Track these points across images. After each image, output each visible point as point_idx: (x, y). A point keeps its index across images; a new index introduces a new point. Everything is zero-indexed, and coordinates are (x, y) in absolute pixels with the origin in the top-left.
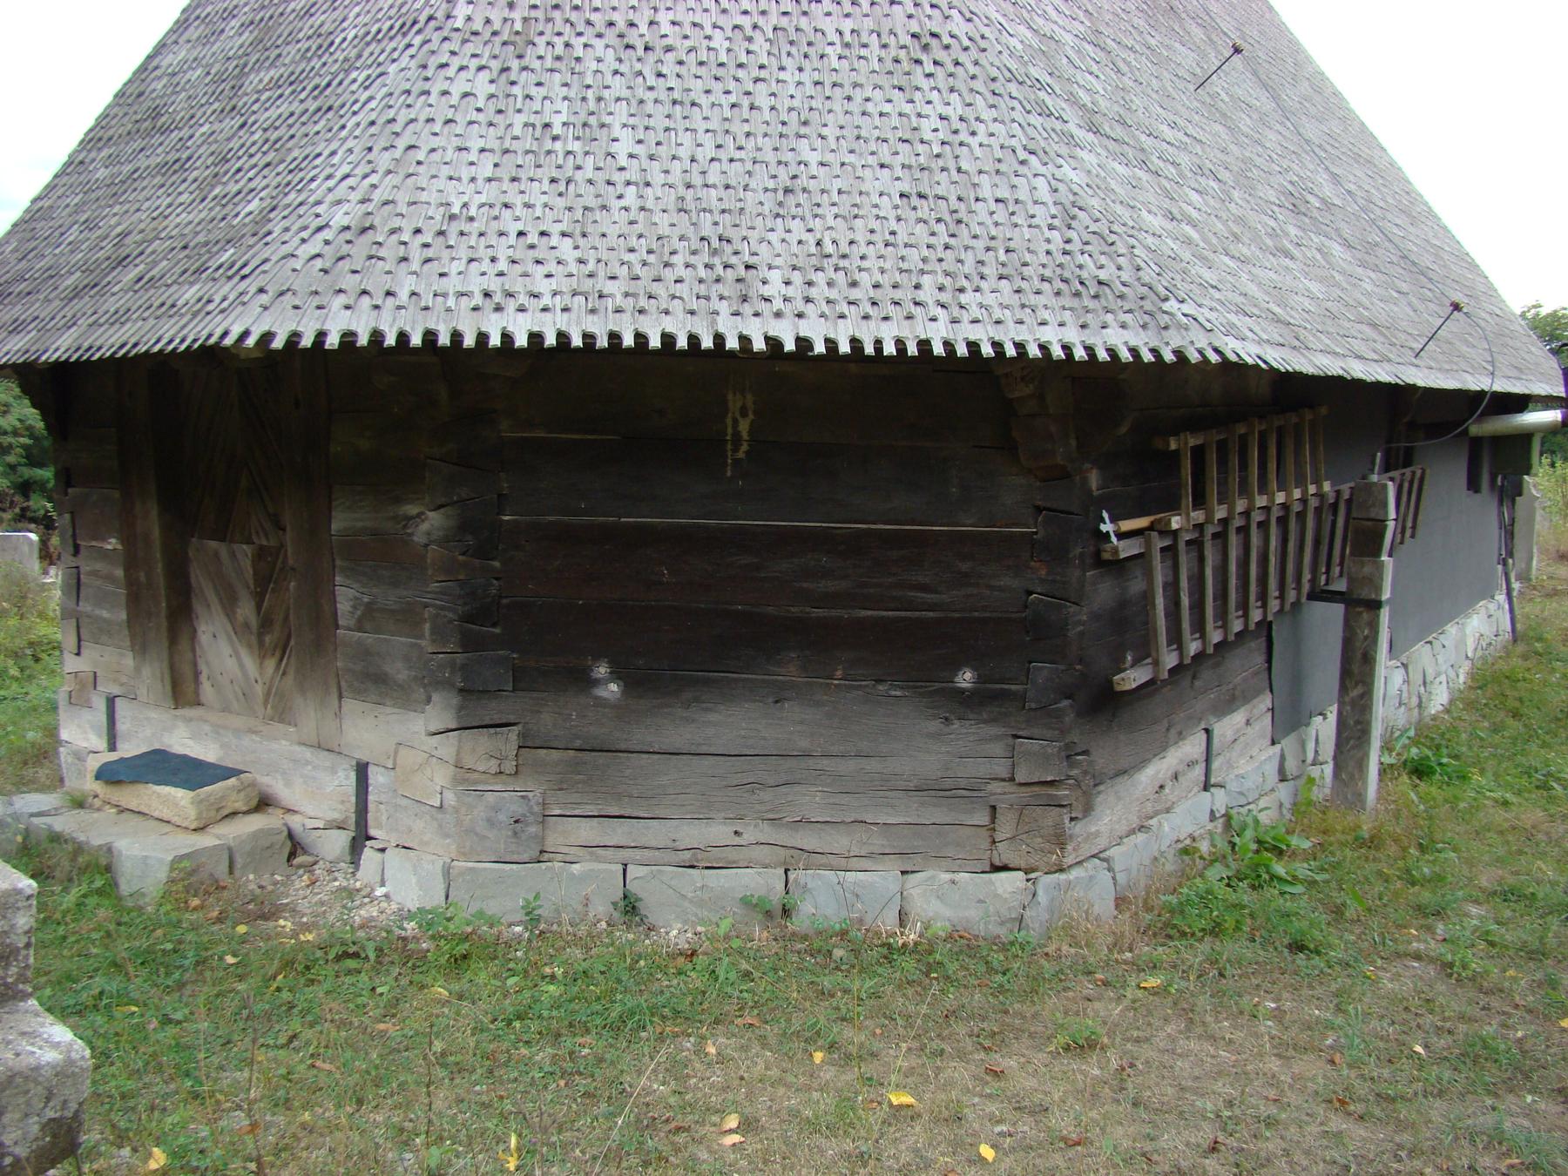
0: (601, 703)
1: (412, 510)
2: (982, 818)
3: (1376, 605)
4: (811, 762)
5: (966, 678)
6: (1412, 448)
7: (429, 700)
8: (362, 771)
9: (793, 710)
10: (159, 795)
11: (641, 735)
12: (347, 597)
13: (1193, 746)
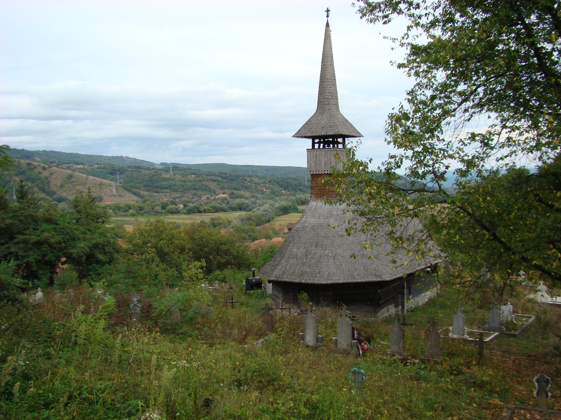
3: (404, 294)
13: (386, 308)
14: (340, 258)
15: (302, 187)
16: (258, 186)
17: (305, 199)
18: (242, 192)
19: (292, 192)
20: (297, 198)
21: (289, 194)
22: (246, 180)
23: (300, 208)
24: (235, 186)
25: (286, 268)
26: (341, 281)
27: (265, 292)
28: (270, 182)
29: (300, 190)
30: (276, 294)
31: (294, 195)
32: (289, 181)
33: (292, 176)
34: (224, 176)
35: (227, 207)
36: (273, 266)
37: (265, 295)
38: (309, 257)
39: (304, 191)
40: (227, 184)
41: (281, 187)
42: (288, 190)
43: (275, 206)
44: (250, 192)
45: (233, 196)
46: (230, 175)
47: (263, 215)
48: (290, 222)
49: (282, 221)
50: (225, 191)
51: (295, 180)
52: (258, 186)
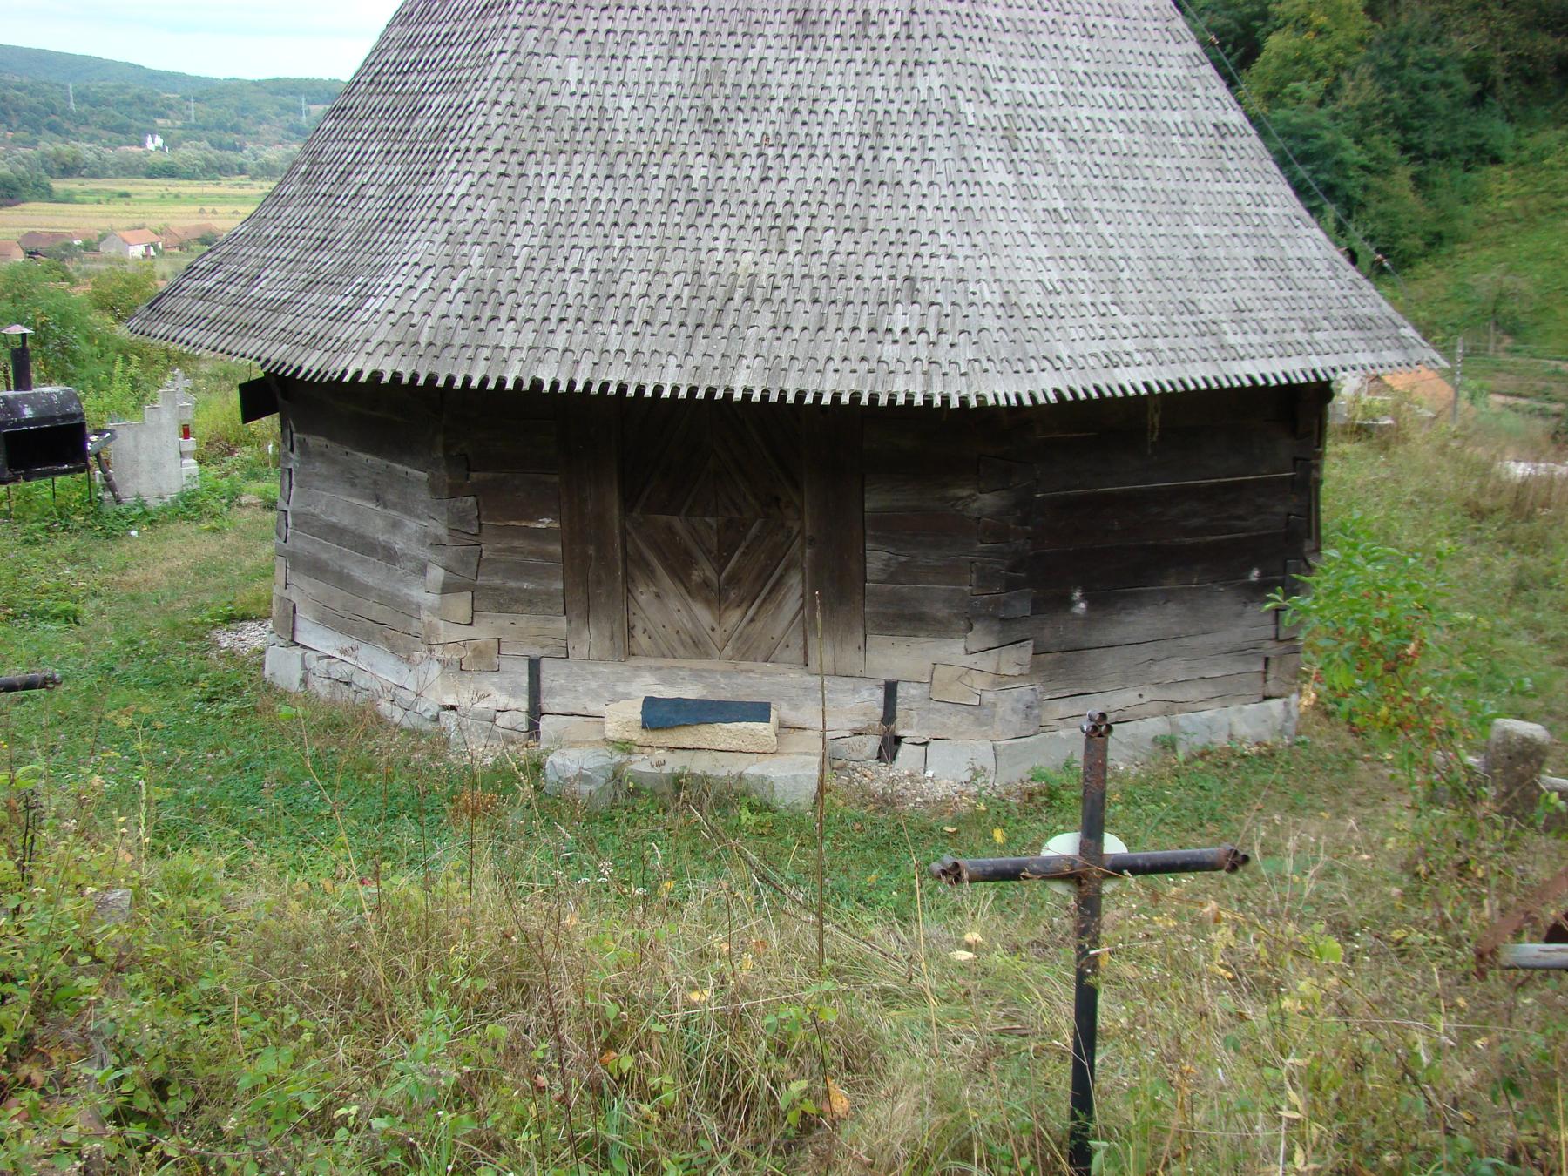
0: (1076, 617)
1: (964, 493)
2: (1260, 667)
4: (1178, 642)
5: (1255, 575)
6: (75, 96)
7: (971, 628)
8: (891, 689)
9: (1172, 608)
10: (729, 731)
11: (1097, 637)
12: (876, 560)
14: (1054, 141)
15: (57, 119)
17: (74, 159)
19: (20, 134)
20: (43, 154)
21: (14, 141)
23: (59, 185)
25: (499, 255)
26: (1131, 379)
27: (110, 486)
29: (53, 128)
30: (345, 520)
31: (34, 144)
32: (10, 93)
33: (17, 79)
36: (322, 244)
37: (109, 509)
38: (747, 131)
39: (68, 132)
42: (10, 125)
48: (26, 230)
51: (31, 94)
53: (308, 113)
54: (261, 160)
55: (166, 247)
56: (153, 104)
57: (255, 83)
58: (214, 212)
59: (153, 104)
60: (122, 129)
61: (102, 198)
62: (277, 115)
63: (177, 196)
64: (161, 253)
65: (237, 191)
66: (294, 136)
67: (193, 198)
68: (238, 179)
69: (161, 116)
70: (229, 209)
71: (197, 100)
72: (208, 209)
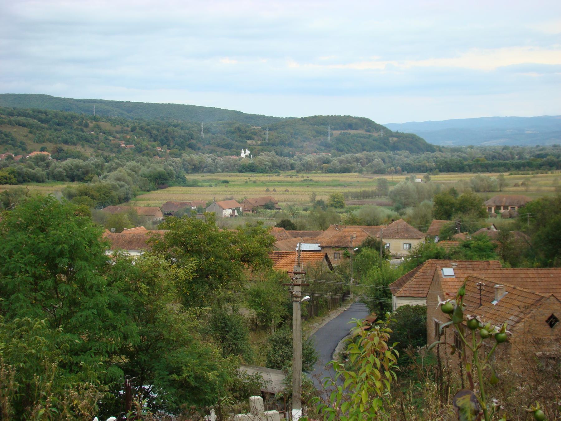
16: (111, 138)
17: (200, 162)
18: (79, 149)
19: (175, 150)
22: (87, 126)
23: (190, 177)
24: (64, 137)
28: (133, 130)
29: (191, 147)
32: (170, 129)
33: (176, 121)
34: (43, 116)
35: (44, 173)
40: (49, 132)
41: (155, 141)
42: (169, 145)
43: (140, 173)
44: (93, 148)
45: (59, 155)
46: (56, 115)
47: (114, 188)
49: (153, 199)
50: (44, 145)
51: (182, 129)
52: (111, 138)
53: (332, 135)
54: (304, 161)
55: (244, 210)
56: (246, 132)
57: (303, 119)
58: (274, 190)
59: (246, 132)
60: (228, 146)
61: (213, 184)
62: (314, 137)
63: (255, 182)
64: (240, 214)
65: (289, 179)
66: (323, 148)
67: (263, 183)
68: (290, 173)
69: (250, 138)
70: (283, 189)
71: (270, 129)
72: (271, 189)
